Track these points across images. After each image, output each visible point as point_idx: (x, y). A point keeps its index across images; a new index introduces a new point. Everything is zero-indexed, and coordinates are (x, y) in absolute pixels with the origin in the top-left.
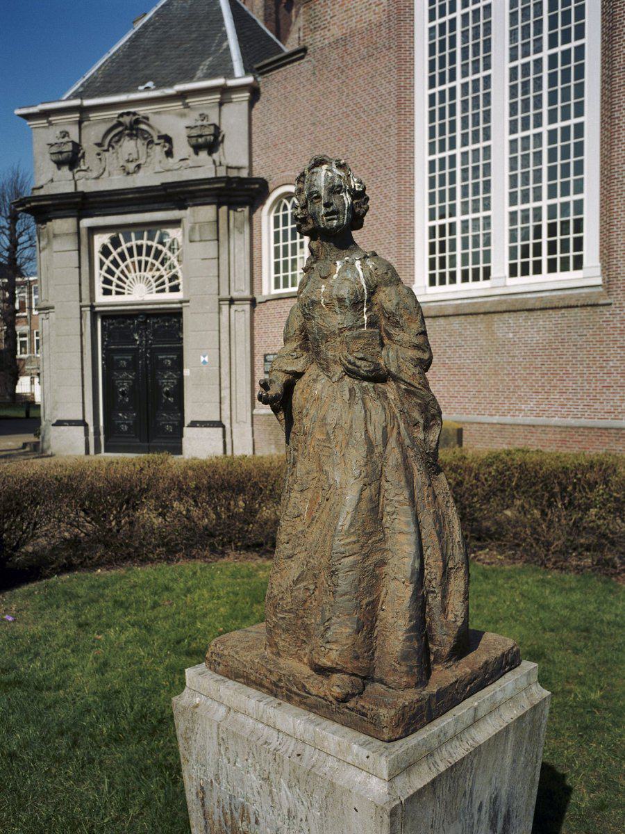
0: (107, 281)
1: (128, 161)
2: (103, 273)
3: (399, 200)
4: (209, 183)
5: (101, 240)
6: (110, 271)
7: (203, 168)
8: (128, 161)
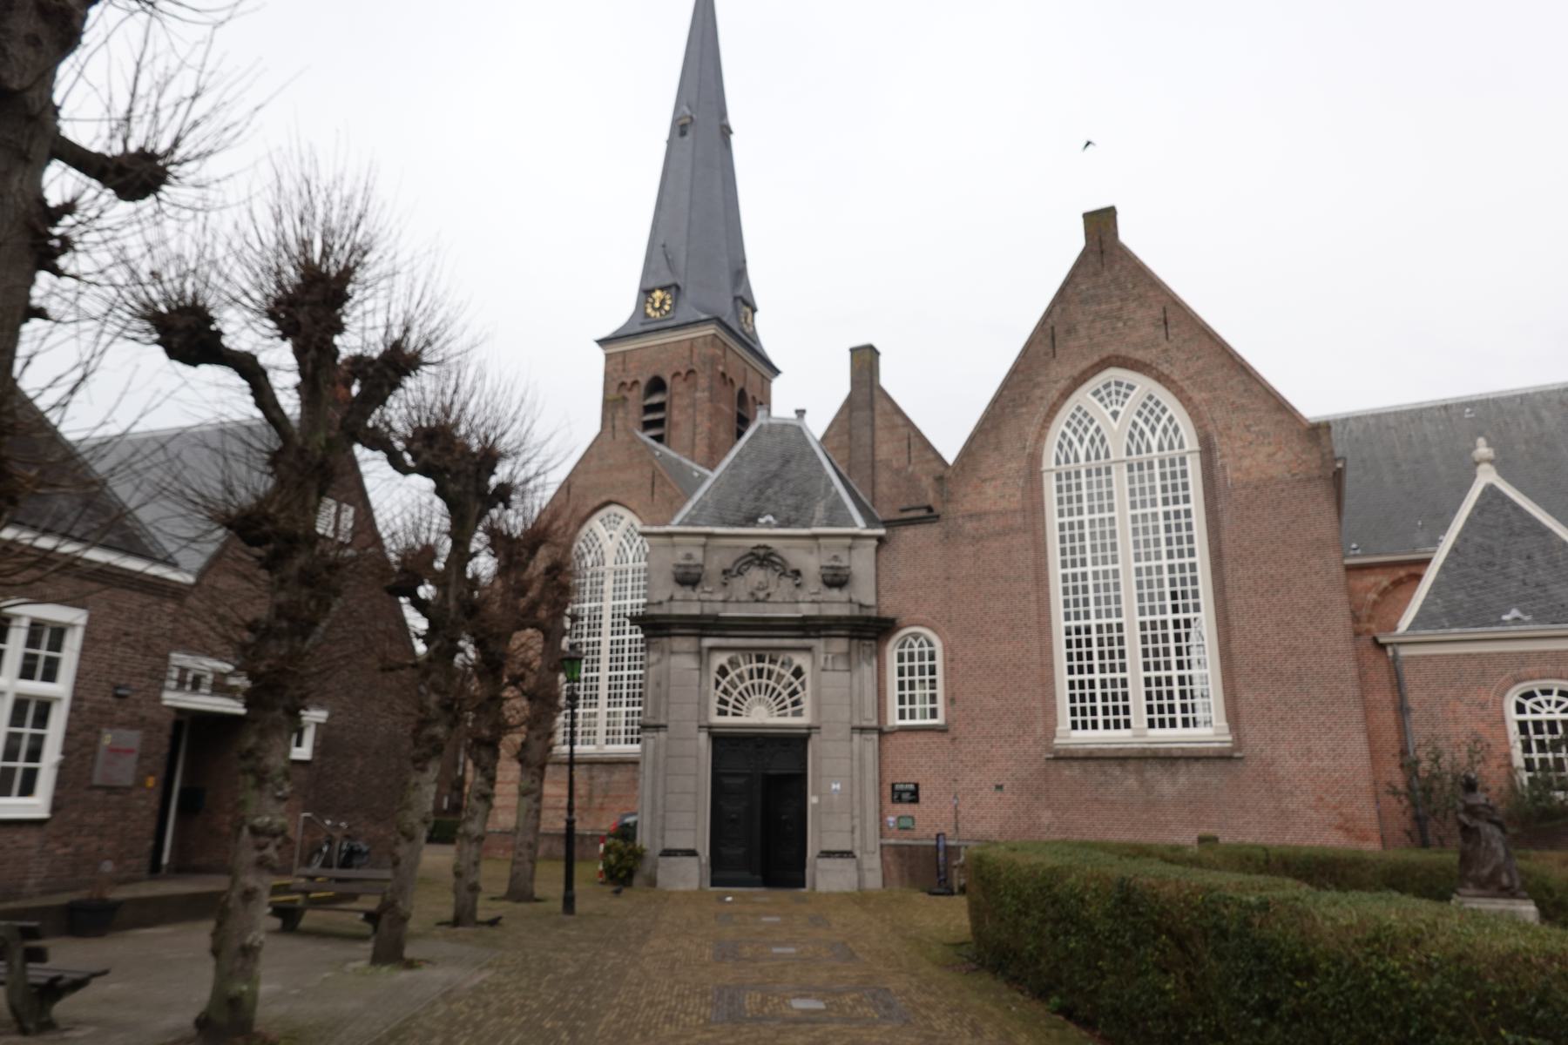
0: (723, 702)
1: (758, 589)
2: (719, 693)
3: (1041, 654)
4: (71, 565)
5: (721, 659)
6: (725, 691)
7: (836, 605)
8: (758, 589)
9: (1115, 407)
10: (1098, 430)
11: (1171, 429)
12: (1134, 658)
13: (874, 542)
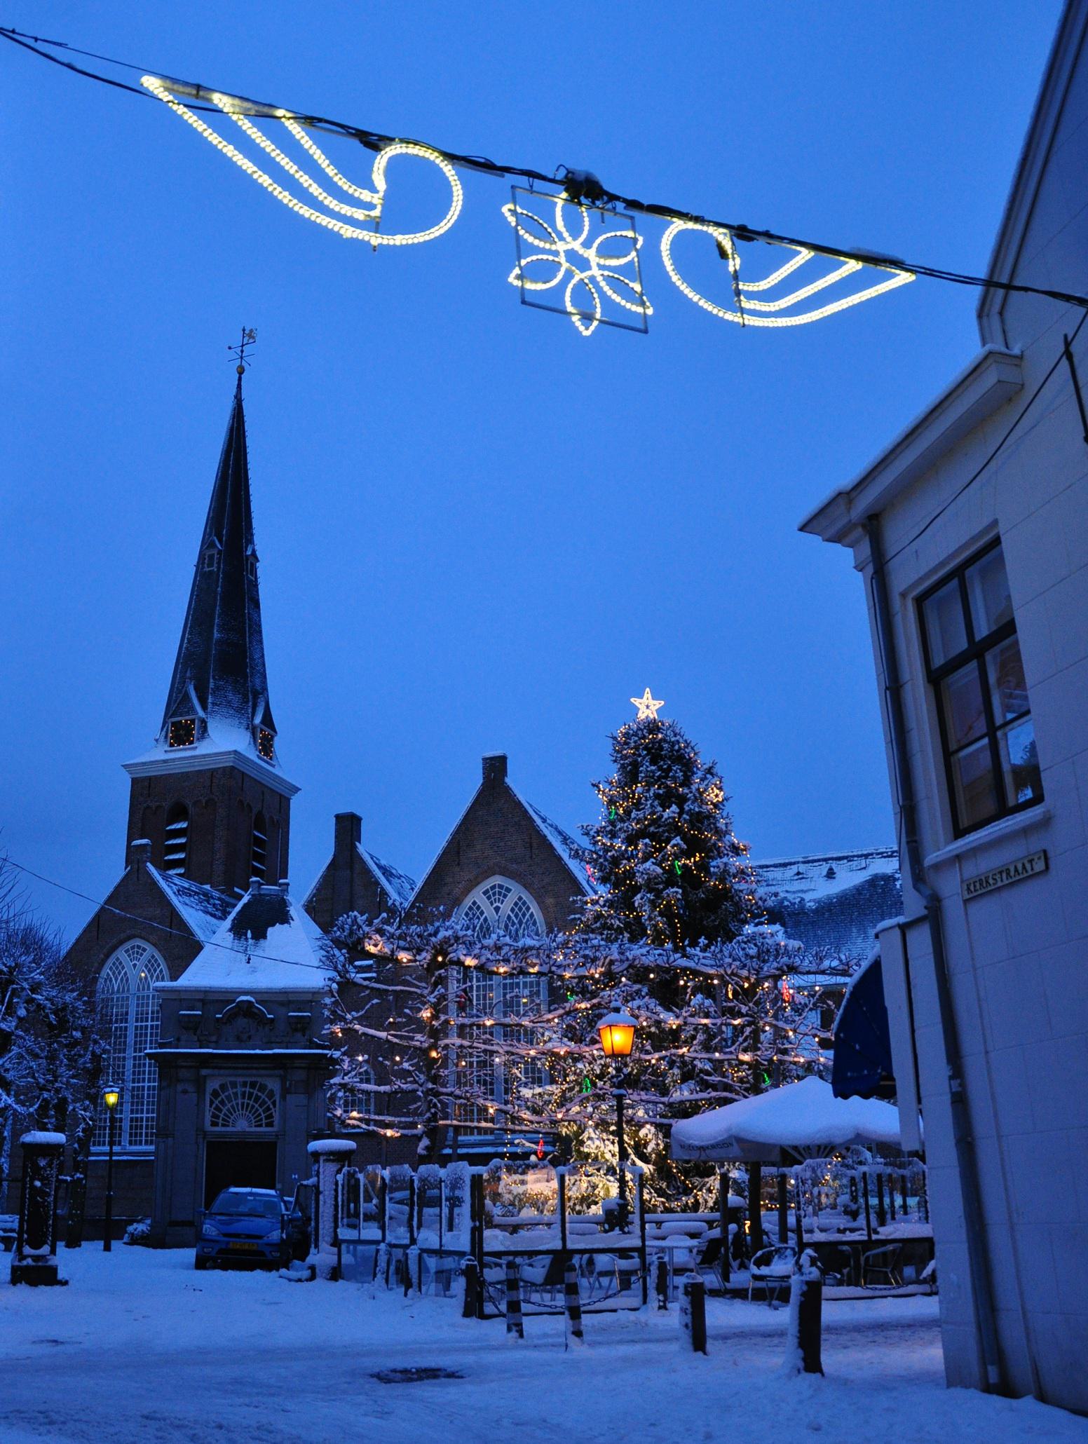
0: (214, 1116)
6: (217, 1108)
10: (125, 973)
13: (897, 932)
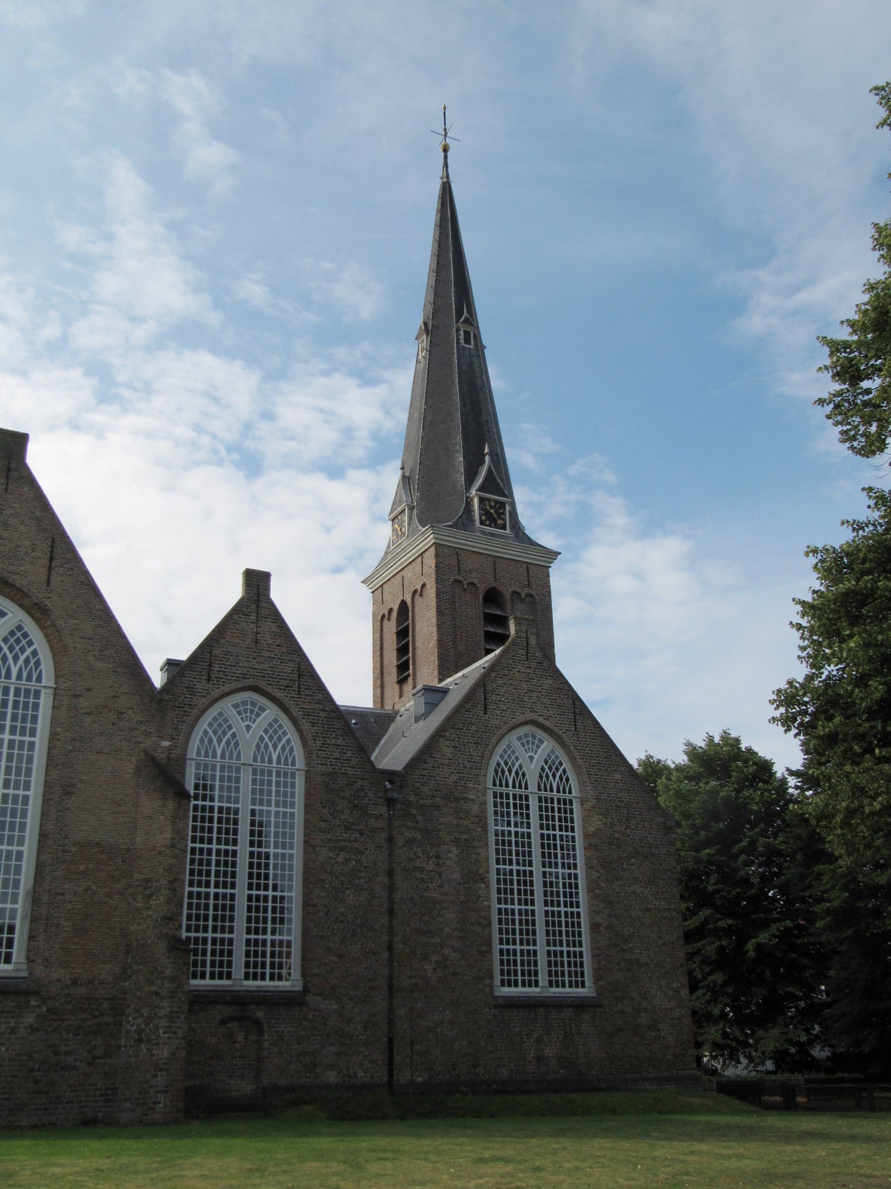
9: (248, 723)
10: (234, 735)
11: (32, 661)
12: (242, 879)
